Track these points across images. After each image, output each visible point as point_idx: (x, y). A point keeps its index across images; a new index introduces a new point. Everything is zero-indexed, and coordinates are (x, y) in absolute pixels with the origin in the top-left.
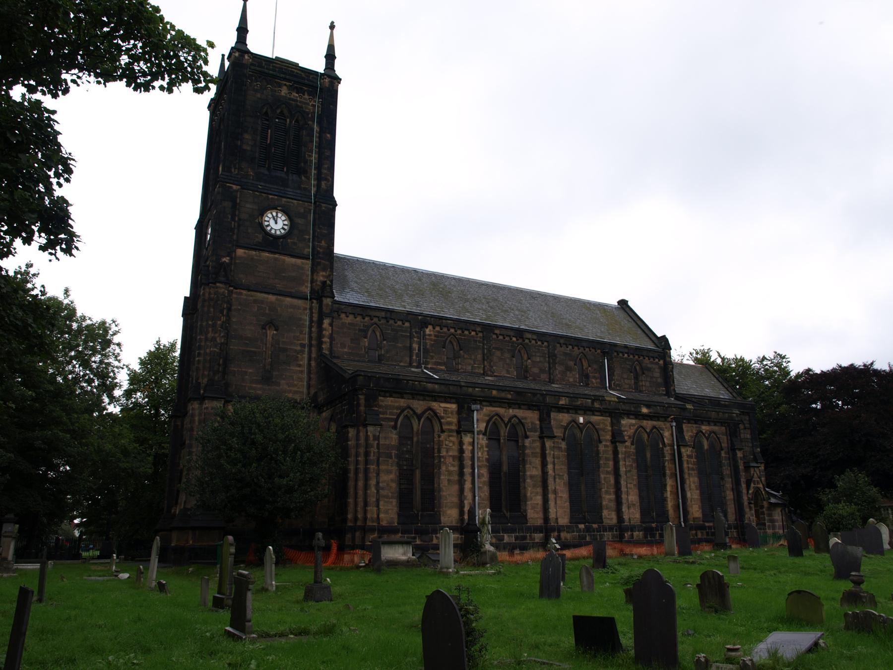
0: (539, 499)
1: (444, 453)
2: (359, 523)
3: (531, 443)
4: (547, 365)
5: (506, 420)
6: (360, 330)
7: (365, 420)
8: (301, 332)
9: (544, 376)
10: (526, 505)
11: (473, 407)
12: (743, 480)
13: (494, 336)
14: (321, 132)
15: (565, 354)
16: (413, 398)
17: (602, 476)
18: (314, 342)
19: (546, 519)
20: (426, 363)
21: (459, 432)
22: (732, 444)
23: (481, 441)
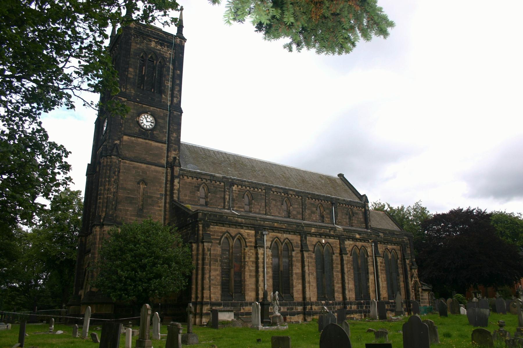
0: (300, 287)
1: (247, 259)
2: (199, 300)
3: (296, 254)
4: (301, 210)
5: (282, 240)
6: (195, 187)
7: (203, 239)
8: (161, 187)
9: (299, 216)
10: (293, 290)
11: (264, 233)
12: (409, 276)
13: (272, 192)
14: (174, 70)
15: (311, 204)
16: (230, 227)
17: (335, 273)
18: (168, 193)
19: (304, 298)
20: (233, 207)
21: (256, 247)
22: (404, 256)
23: (268, 253)
